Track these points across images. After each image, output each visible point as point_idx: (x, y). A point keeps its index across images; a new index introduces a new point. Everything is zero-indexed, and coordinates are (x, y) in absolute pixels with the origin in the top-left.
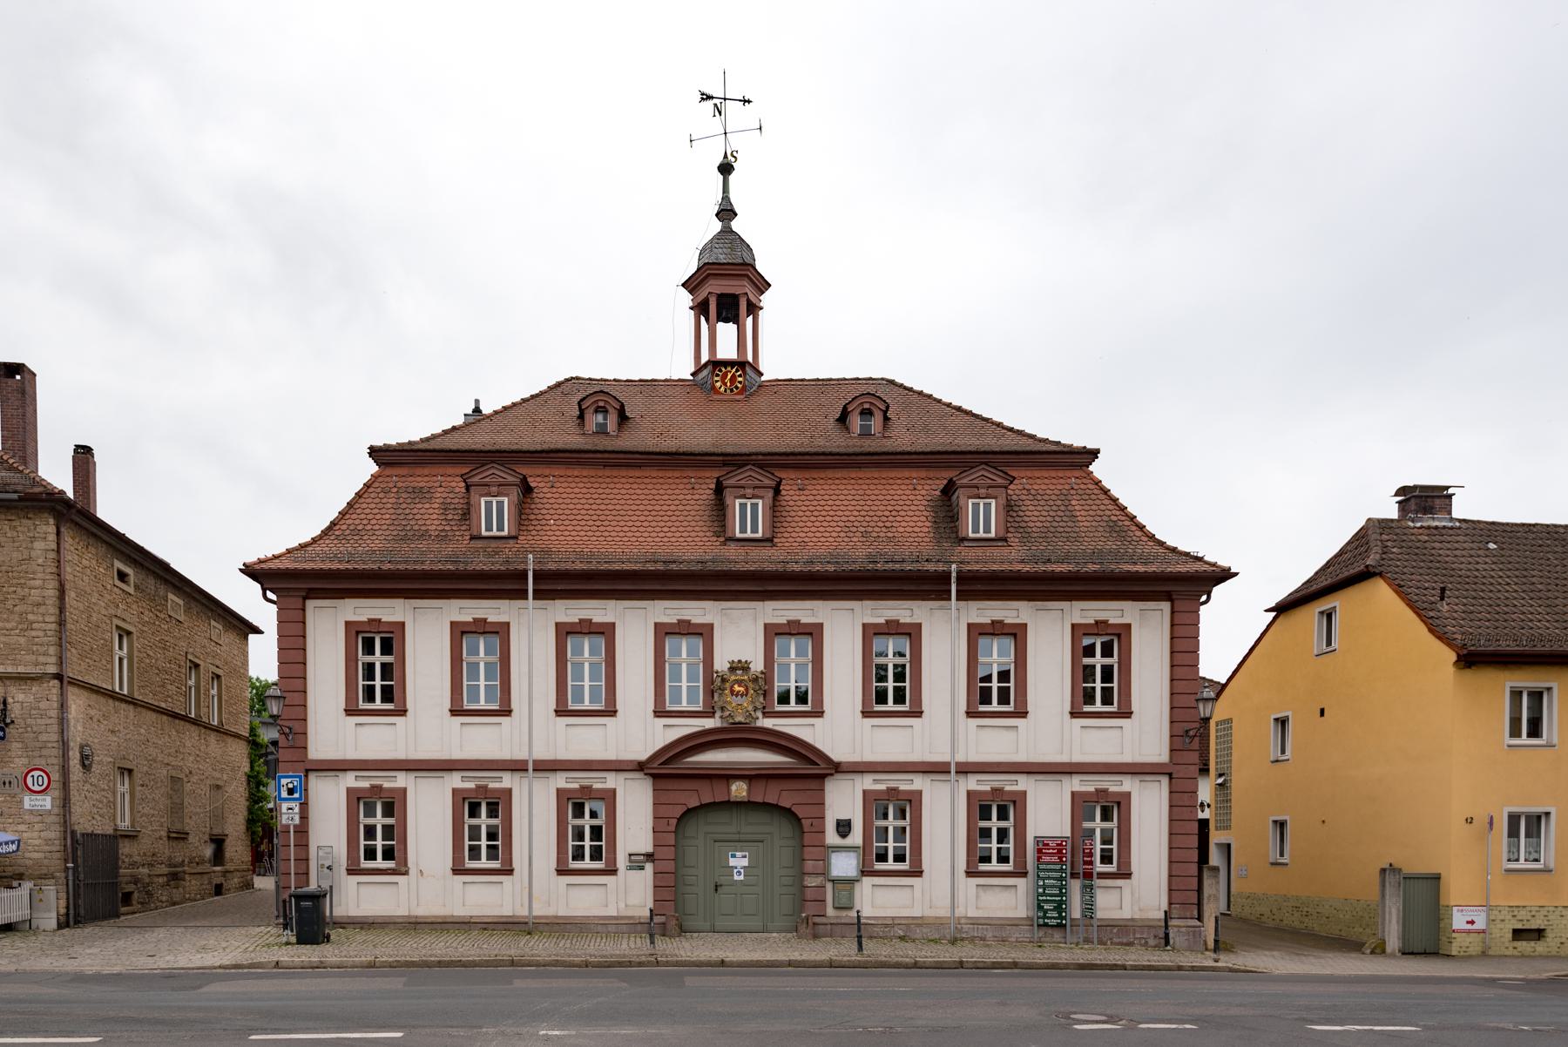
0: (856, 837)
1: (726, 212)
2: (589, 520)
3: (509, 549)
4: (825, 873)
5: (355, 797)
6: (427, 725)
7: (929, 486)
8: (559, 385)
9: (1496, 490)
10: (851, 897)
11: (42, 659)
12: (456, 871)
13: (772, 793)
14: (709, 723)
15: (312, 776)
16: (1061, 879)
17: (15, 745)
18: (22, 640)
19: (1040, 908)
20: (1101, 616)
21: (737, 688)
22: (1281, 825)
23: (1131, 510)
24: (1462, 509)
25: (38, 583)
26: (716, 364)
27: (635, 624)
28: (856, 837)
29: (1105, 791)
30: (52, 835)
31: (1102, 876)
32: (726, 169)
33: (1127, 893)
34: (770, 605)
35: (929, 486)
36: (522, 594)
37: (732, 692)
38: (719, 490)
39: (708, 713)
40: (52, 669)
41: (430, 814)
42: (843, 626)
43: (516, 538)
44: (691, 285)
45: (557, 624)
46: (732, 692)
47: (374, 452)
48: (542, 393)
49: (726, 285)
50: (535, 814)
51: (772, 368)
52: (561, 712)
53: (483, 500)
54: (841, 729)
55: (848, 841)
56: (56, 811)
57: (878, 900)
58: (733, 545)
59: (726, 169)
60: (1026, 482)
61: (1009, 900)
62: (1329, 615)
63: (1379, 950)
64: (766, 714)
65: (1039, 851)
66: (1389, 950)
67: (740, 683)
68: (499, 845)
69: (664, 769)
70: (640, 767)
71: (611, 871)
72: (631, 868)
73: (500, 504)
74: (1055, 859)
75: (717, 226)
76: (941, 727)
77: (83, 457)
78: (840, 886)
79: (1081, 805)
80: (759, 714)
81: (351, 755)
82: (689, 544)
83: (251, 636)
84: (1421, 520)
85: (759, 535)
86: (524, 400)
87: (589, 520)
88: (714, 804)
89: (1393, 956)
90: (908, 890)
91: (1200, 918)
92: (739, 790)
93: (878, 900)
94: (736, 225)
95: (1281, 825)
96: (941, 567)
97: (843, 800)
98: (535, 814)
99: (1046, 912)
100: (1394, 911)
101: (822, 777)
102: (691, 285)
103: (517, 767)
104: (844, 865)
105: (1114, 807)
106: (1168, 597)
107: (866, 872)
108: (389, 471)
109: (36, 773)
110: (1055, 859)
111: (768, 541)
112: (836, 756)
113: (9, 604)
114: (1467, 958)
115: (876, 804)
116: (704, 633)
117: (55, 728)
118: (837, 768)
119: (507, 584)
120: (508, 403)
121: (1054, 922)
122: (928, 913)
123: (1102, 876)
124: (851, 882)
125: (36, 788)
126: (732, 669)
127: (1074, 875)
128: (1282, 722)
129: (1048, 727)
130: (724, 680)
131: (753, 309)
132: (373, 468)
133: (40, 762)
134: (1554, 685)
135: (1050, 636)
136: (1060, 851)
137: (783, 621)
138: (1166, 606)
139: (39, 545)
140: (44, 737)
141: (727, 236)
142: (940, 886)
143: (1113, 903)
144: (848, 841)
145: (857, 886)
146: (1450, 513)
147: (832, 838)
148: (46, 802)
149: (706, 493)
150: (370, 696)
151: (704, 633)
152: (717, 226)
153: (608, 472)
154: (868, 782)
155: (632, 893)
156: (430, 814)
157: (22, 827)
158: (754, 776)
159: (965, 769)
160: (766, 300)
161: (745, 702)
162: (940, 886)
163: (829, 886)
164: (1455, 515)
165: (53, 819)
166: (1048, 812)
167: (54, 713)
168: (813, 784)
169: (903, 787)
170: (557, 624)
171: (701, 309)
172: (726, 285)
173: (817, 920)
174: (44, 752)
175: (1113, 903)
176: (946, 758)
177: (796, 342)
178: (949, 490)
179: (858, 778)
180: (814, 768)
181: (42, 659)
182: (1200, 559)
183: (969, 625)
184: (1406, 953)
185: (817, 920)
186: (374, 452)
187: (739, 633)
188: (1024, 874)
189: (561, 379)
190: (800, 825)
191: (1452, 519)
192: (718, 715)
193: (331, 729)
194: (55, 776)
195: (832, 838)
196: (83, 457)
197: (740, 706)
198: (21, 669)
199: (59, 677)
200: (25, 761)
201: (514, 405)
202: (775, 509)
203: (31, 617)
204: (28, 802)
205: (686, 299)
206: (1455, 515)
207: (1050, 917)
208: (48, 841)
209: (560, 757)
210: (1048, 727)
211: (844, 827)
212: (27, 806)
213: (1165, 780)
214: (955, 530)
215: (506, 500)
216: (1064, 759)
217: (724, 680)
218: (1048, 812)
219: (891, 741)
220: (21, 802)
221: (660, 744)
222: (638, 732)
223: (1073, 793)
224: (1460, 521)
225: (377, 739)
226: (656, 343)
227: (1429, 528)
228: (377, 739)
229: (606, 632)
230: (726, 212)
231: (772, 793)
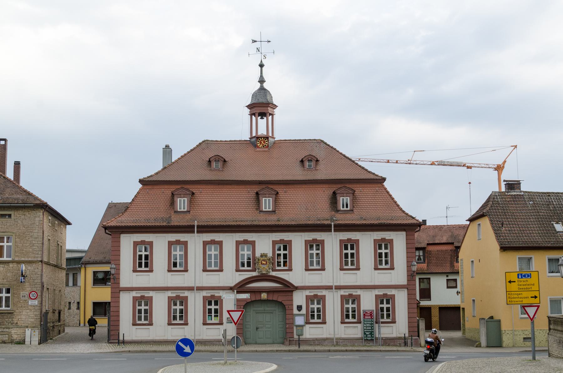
0: (304, 311)
1: (262, 81)
2: (216, 206)
3: (188, 217)
4: (293, 323)
5: (135, 299)
6: (160, 275)
7: (327, 192)
8: (200, 144)
9: (536, 181)
10: (302, 330)
11: (36, 256)
12: (134, 325)
13: (275, 297)
14: (254, 274)
15: (121, 293)
16: (372, 324)
17: (27, 284)
18: (31, 250)
19: (365, 334)
20: (383, 236)
21: (263, 262)
22: (474, 300)
23: (396, 199)
24: (524, 188)
25: (36, 231)
26: (258, 138)
27: (229, 241)
28: (304, 311)
29: (386, 294)
30: (37, 313)
31: (383, 323)
32: (261, 66)
33: (394, 328)
34: (274, 234)
35: (327, 192)
36: (193, 232)
37: (262, 263)
38: (257, 194)
39: (254, 270)
40: (40, 259)
41: (160, 305)
42: (298, 241)
43: (189, 212)
44: (249, 107)
45: (203, 241)
46: (262, 263)
47: (141, 181)
48: (194, 148)
49: (261, 107)
50: (195, 305)
51: (278, 136)
52: (205, 270)
53: (178, 199)
54: (297, 275)
55: (301, 312)
56: (39, 305)
57: (311, 332)
58: (262, 213)
59: (261, 66)
60: (359, 190)
61: (355, 331)
62: (479, 225)
63: (479, 346)
64: (273, 271)
65: (364, 315)
66: (482, 346)
67: (264, 260)
68: (183, 314)
69: (240, 288)
70: (231, 289)
71: (221, 323)
72: (228, 323)
73: (184, 201)
74: (370, 317)
75: (258, 85)
76: (332, 274)
77: (17, 165)
78: (298, 328)
79: (380, 299)
80: (271, 270)
81: (135, 285)
82: (247, 215)
83: (67, 226)
84: (510, 192)
85: (271, 210)
86: (188, 152)
87: (216, 206)
88: (256, 301)
89: (483, 347)
90: (321, 329)
91: (419, 336)
92: (264, 296)
93: (311, 332)
94: (265, 85)
95: (474, 300)
96: (329, 222)
97: (299, 299)
98: (195, 305)
99: (367, 335)
100: (483, 332)
101: (292, 291)
102: (249, 107)
103: (191, 289)
104: (300, 321)
105: (390, 299)
106: (404, 230)
107: (307, 323)
108: (145, 187)
109: (33, 293)
110: (370, 317)
111: (274, 212)
112: (296, 285)
113: (27, 238)
114: (508, 347)
115: (310, 299)
116: (253, 243)
117: (40, 278)
118: (297, 288)
119: (188, 229)
120: (183, 154)
121: (370, 338)
122: (328, 336)
123: (383, 323)
124: (302, 326)
125: (33, 298)
126: (262, 256)
127: (376, 323)
128: (472, 261)
129: (367, 273)
130: (259, 260)
131: (272, 115)
132: (140, 186)
133: (35, 289)
134: (533, 256)
135: (366, 242)
136: (371, 315)
137: (279, 239)
138: (404, 233)
139: (37, 219)
140: (36, 281)
141: (262, 89)
142: (334, 327)
143: (386, 331)
144: (301, 312)
145: (304, 327)
146: (520, 189)
147: (295, 311)
148: (36, 302)
149: (253, 195)
150: (140, 266)
151: (253, 243)
152: (258, 85)
153: (220, 186)
154: (308, 293)
155: (231, 330)
156: (160, 305)
157: (28, 311)
158: (269, 291)
159: (339, 288)
160: (276, 111)
161: (266, 267)
162: (334, 327)
163: (295, 328)
164: (522, 190)
165: (37, 308)
166: (368, 302)
167: (39, 273)
168: (290, 294)
169: (319, 294)
170: (203, 241)
171: (252, 114)
172: (261, 107)
173: (291, 339)
174: (36, 286)
175: (386, 331)
176: (331, 284)
177: (286, 125)
178: (334, 193)
179: (304, 291)
180: (288, 288)
181: (36, 256)
182: (414, 218)
183: (340, 240)
184: (488, 347)
185: (291, 339)
186: (141, 181)
187: (264, 244)
188: (360, 323)
189: (201, 141)
190: (285, 308)
191: (521, 192)
192: (257, 271)
193: (128, 277)
194: (39, 294)
195: (295, 311)
196: (17, 165)
197: (264, 268)
198: (30, 259)
199: (41, 261)
200: (30, 289)
201: (185, 155)
202: (276, 201)
203: (34, 242)
204: (30, 302)
205: (248, 111)
206: (522, 190)
207: (369, 337)
208: (36, 315)
209: (204, 285)
210: (367, 273)
211: (299, 308)
212: (30, 304)
213: (406, 290)
214: (336, 207)
215: (186, 199)
216: (372, 284)
217: (259, 260)
218: (368, 302)
219: (314, 279)
220: (28, 302)
221: (238, 281)
222: (231, 276)
223: (376, 295)
224: (524, 192)
225: (142, 280)
226: (237, 126)
227: (512, 195)
228: (142, 280)
229: (220, 243)
230: (262, 81)
231: (275, 297)
